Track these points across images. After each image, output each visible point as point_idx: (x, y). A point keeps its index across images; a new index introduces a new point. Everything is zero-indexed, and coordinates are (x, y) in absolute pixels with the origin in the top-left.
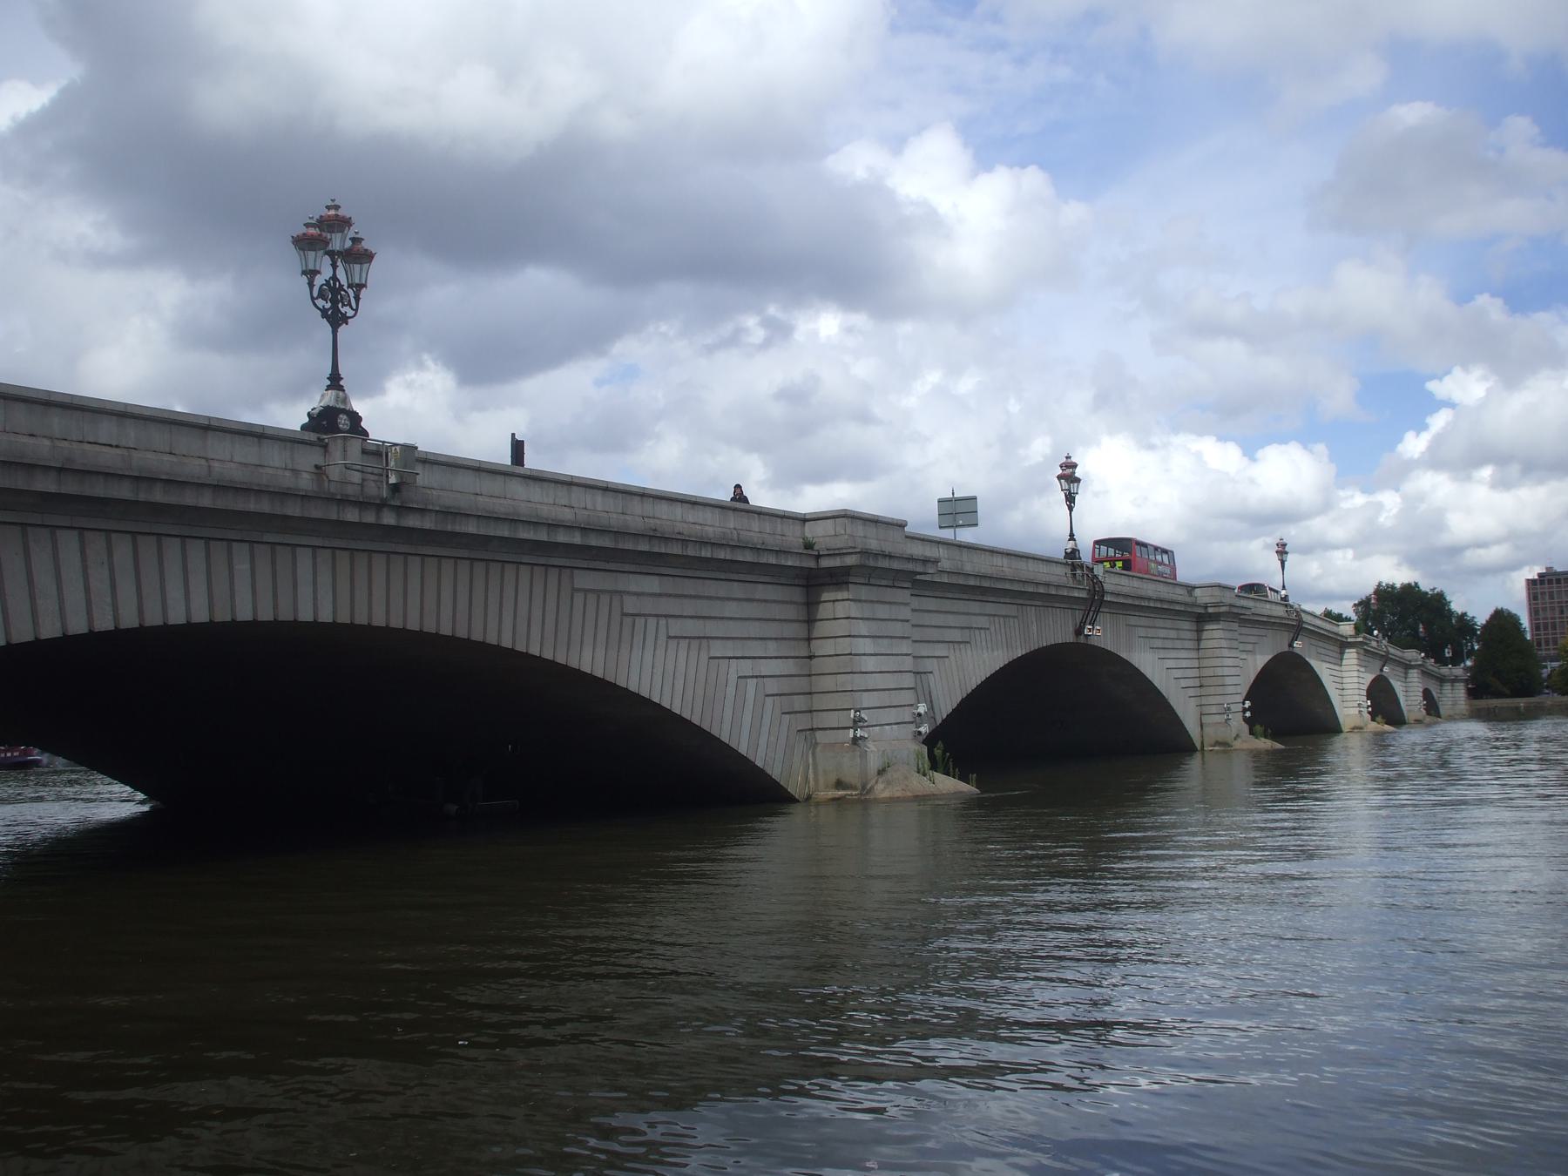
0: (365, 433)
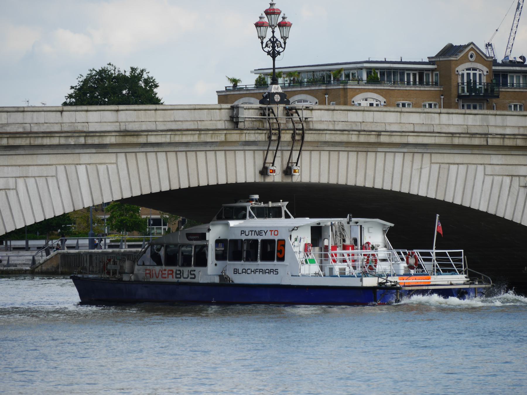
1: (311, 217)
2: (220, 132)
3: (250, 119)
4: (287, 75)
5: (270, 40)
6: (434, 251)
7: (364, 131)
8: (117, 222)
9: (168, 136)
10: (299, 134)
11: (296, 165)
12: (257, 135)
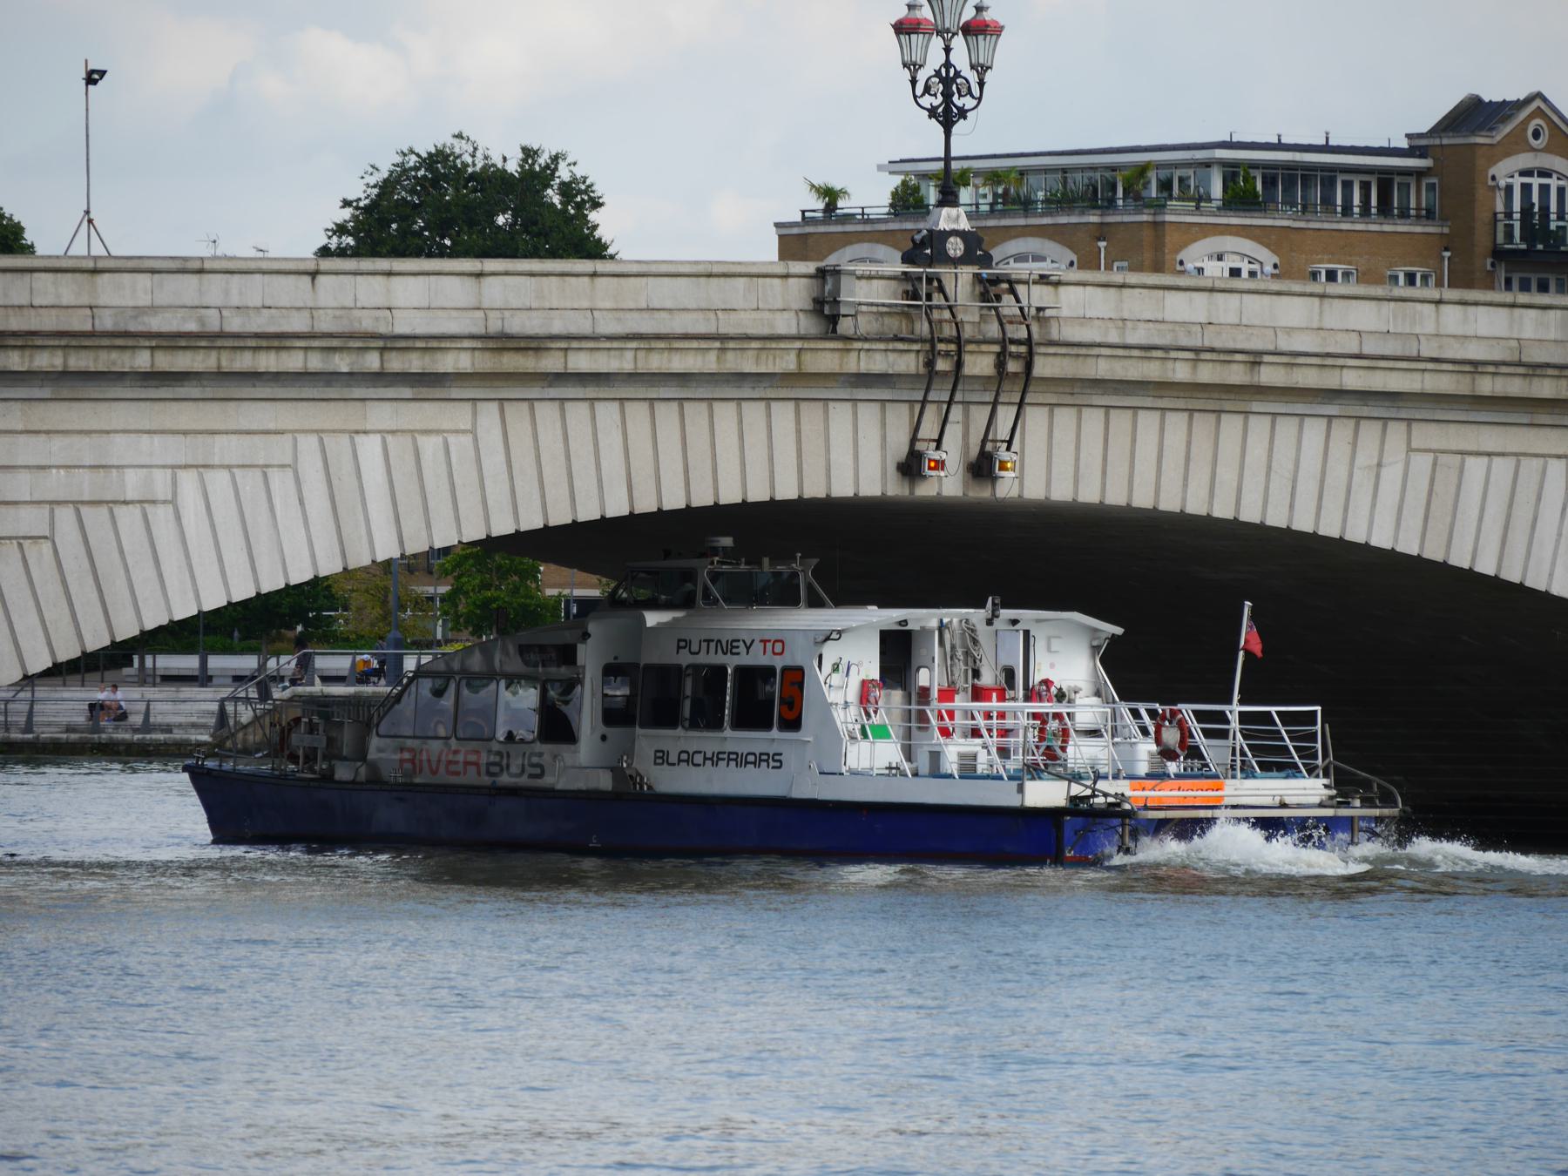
1: (882, 605)
2: (782, 345)
3: (874, 309)
4: (987, 179)
5: (938, 73)
6: (1234, 709)
7: (1212, 350)
8: (472, 608)
9: (629, 355)
10: (1017, 356)
11: (1008, 449)
12: (891, 356)
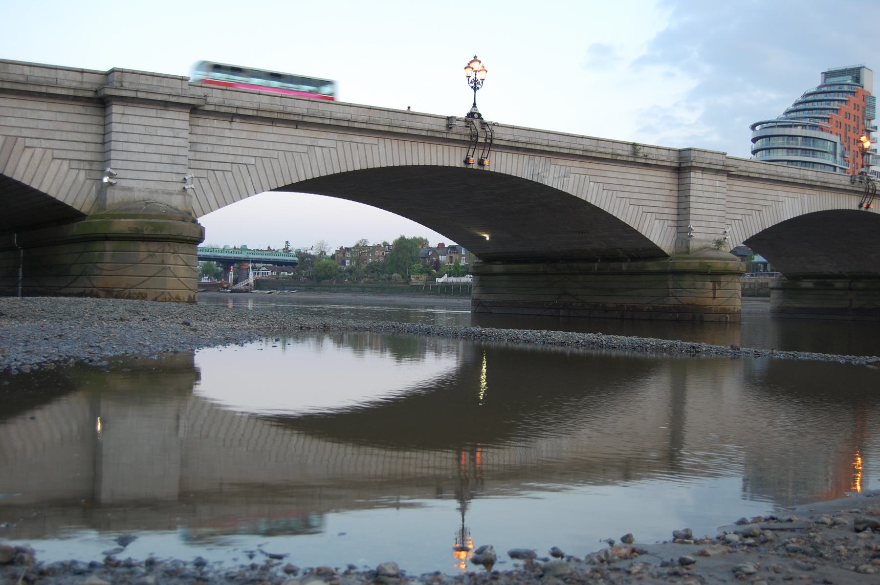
0: (482, 119)
5: (474, 79)
